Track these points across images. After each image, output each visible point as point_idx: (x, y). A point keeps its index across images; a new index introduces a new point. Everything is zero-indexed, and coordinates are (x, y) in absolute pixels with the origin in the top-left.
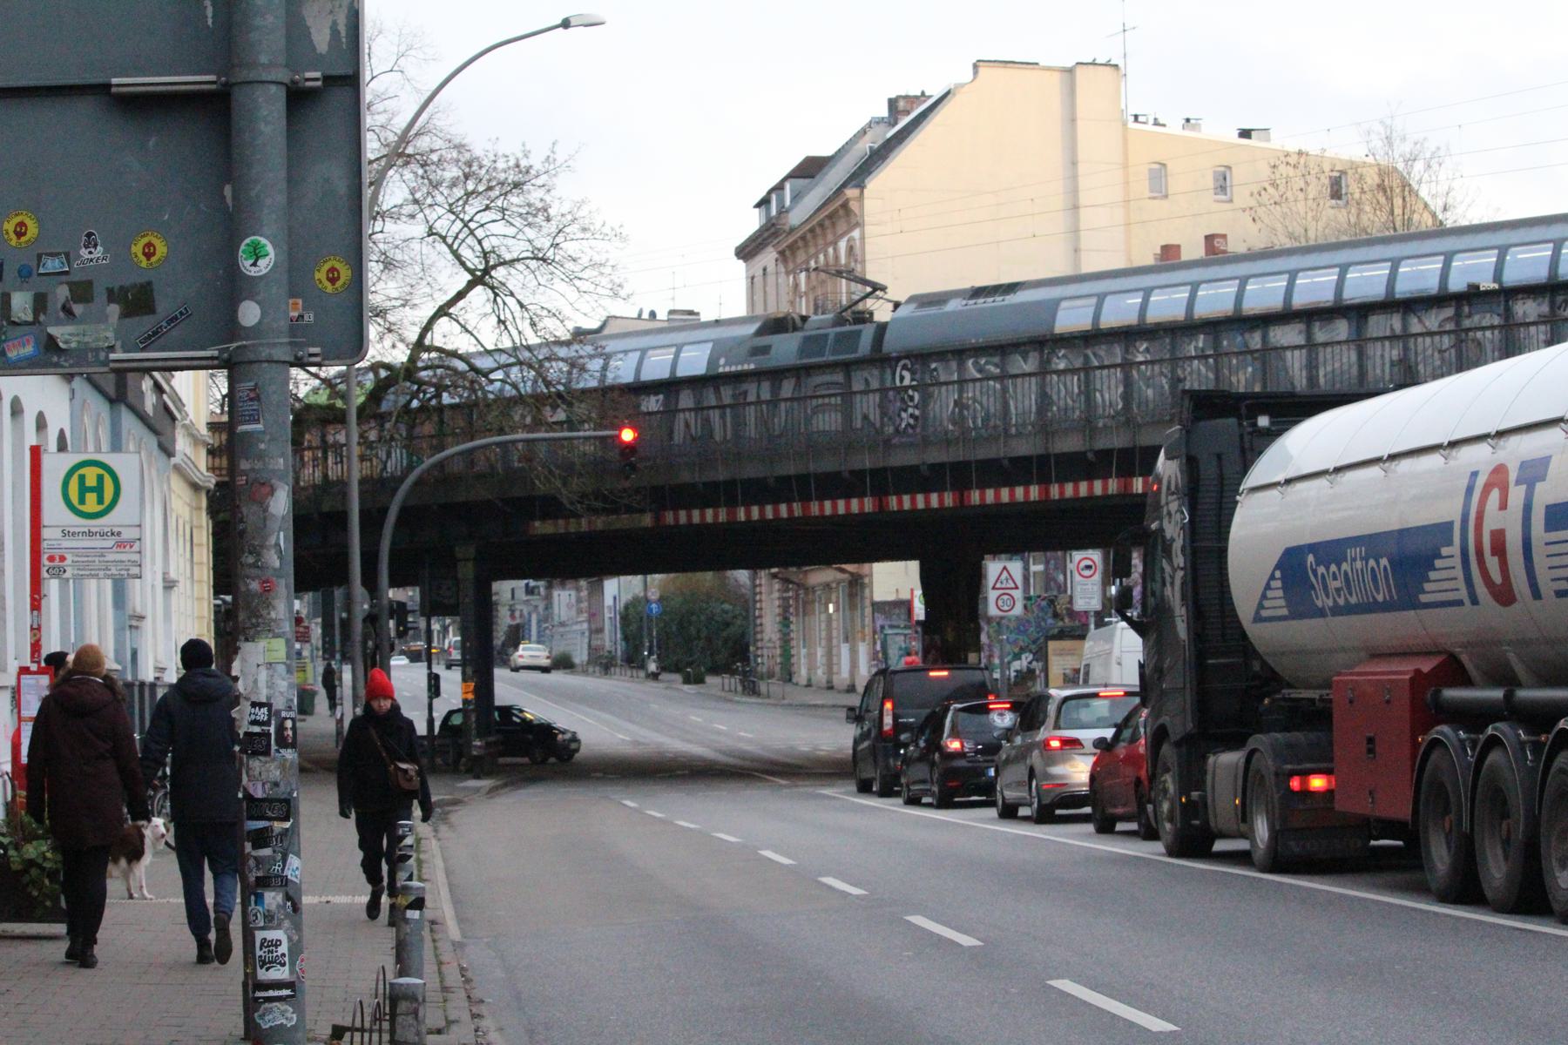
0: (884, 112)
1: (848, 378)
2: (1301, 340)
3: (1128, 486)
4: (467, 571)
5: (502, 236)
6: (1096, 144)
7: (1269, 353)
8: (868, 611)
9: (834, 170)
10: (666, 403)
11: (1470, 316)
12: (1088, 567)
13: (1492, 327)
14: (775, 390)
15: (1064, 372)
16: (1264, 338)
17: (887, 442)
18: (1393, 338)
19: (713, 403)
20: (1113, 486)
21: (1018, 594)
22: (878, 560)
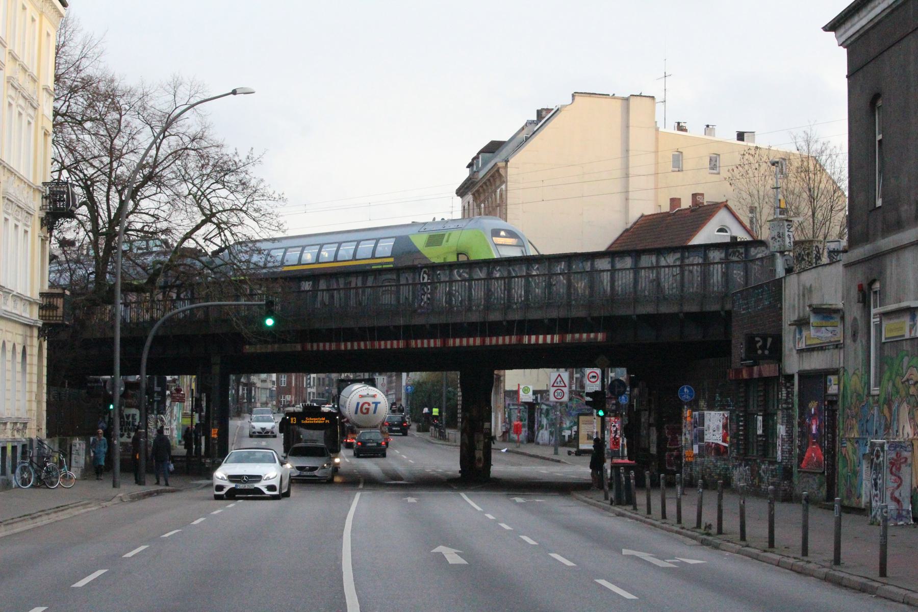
0: (535, 118)
1: (398, 276)
2: (608, 267)
3: (521, 340)
4: (216, 369)
5: (221, 197)
6: (640, 139)
7: (594, 272)
8: (502, 395)
9: (504, 151)
10: (313, 286)
11: (688, 258)
12: (594, 377)
13: (697, 264)
14: (364, 282)
15: (537, 275)
16: (592, 265)
17: (415, 311)
18: (651, 268)
19: (335, 287)
20: (514, 339)
21: (566, 390)
22: (511, 368)
